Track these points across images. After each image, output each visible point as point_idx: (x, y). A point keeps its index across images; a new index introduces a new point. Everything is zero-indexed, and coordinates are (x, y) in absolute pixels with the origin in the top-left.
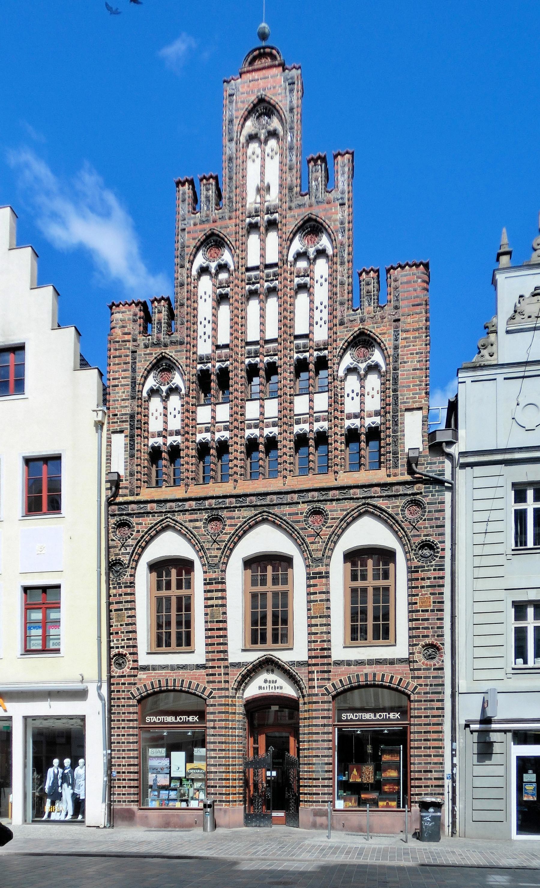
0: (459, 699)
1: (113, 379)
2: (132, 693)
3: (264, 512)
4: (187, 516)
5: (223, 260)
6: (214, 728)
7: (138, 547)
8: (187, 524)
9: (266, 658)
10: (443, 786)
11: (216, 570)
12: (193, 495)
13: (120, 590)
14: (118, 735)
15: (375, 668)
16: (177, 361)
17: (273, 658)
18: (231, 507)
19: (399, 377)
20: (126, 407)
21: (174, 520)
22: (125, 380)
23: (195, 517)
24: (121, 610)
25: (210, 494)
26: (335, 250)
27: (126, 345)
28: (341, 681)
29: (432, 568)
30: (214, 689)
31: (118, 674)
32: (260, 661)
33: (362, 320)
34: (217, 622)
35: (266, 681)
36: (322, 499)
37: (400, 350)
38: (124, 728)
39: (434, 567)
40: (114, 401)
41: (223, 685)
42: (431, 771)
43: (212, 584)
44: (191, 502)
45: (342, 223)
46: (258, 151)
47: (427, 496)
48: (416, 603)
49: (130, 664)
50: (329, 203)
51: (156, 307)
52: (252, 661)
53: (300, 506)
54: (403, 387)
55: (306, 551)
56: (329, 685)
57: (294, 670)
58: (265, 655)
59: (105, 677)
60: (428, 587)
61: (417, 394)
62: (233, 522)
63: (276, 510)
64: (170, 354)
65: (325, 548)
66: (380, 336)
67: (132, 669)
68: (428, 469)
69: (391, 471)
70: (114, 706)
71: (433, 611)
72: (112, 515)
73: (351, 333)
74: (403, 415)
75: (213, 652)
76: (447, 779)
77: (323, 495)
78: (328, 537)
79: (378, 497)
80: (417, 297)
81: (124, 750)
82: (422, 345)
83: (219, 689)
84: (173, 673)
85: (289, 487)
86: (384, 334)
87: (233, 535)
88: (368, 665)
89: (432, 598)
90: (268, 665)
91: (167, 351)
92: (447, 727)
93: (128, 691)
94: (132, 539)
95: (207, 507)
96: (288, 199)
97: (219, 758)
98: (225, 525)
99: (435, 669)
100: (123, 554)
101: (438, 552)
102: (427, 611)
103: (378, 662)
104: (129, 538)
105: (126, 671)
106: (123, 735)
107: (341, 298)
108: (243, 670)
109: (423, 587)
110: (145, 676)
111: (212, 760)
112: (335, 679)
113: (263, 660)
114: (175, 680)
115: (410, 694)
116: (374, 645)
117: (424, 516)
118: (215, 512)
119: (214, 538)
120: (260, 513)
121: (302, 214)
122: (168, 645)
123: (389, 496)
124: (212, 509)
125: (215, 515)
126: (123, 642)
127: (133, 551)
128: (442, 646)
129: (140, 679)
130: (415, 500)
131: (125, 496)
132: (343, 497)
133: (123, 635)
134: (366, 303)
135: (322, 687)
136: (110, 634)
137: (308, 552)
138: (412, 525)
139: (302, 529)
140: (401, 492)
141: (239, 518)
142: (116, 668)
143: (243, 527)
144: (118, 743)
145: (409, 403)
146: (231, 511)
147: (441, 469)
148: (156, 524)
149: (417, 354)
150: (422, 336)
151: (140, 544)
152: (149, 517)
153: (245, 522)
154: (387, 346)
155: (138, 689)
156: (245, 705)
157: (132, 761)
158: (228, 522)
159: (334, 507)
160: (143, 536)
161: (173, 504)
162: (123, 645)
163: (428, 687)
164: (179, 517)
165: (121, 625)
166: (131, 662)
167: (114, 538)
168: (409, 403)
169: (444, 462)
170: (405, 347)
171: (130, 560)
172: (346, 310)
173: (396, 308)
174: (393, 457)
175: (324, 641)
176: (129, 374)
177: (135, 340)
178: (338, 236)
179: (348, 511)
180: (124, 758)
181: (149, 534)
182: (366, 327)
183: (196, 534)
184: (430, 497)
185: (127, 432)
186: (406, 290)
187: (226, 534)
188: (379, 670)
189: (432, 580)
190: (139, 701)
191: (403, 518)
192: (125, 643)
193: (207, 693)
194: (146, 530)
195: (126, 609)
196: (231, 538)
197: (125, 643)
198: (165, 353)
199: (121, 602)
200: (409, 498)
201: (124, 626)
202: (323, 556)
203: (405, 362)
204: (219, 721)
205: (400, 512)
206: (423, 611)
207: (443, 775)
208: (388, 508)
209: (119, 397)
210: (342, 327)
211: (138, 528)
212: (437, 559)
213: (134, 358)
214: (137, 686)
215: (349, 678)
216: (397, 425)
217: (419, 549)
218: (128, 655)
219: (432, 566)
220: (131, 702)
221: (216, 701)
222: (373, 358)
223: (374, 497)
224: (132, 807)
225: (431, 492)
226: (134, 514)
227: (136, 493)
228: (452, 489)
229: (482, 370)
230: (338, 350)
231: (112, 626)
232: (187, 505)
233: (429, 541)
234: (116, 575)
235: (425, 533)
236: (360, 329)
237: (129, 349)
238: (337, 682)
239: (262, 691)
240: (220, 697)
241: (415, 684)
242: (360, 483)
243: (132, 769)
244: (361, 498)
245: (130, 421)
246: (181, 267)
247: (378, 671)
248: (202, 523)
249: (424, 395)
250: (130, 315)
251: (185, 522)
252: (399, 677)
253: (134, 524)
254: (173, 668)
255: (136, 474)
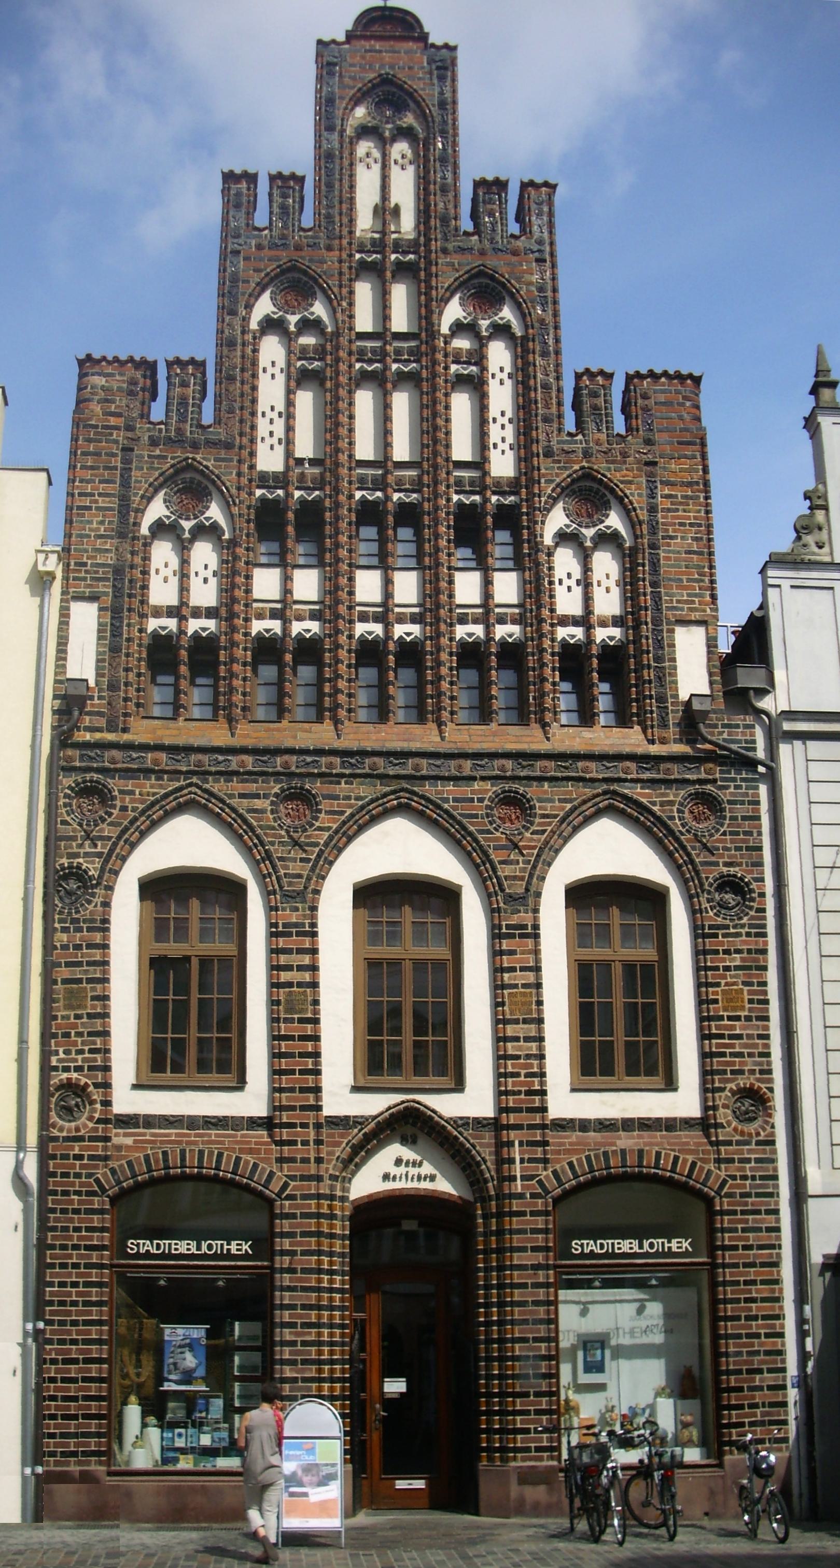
0: (813, 1207)
1: (80, 495)
2: (97, 1181)
3: (402, 790)
4: (235, 784)
5: (313, 314)
6: (292, 1271)
7: (122, 843)
8: (234, 802)
9: (406, 1108)
10: (784, 1404)
11: (300, 905)
12: (249, 743)
13: (78, 935)
14: (62, 1284)
15: (639, 1137)
16: (219, 478)
17: (422, 1108)
18: (331, 775)
19: (662, 562)
20: (107, 551)
21: (206, 791)
22: (107, 499)
23: (252, 787)
24: (80, 981)
25: (289, 743)
26: (531, 331)
27: (111, 434)
28: (571, 1164)
29: (743, 931)
30: (293, 1178)
31: (65, 1134)
32: (392, 1115)
33: (587, 454)
34: (301, 1021)
35: (398, 1162)
36: (522, 774)
37: (659, 515)
38: (76, 1266)
39: (747, 930)
40: (81, 536)
41: (312, 1169)
42: (760, 1371)
43: (289, 934)
44: (245, 757)
45: (541, 289)
46: (376, 154)
47: (727, 787)
48: (716, 1001)
49: (95, 1110)
50: (515, 253)
51: (177, 375)
52: (374, 1113)
53: (476, 786)
54: (670, 579)
55: (491, 879)
56: (545, 1174)
57: (466, 1137)
58: (403, 1102)
59: (32, 1138)
60: (737, 968)
61: (696, 595)
62: (335, 805)
63: (428, 789)
64: (205, 463)
65: (531, 876)
66: (621, 486)
67: (99, 1121)
68: (725, 736)
69: (656, 733)
70: (53, 1211)
71: (748, 1019)
72: (63, 769)
73: (568, 472)
74: (672, 631)
75: (292, 1090)
76: (793, 1387)
77: (523, 767)
78: (536, 852)
79: (632, 781)
80: (687, 430)
81: (74, 1323)
82: (699, 511)
83: (303, 1178)
84: (196, 1135)
85: (452, 745)
86: (630, 482)
87: (336, 832)
88: (624, 1130)
89: (745, 993)
90: (406, 1123)
91: (198, 457)
92: (787, 1271)
93: (89, 1176)
94: (109, 825)
95: (279, 769)
96: (439, 236)
97: (304, 1343)
98: (320, 811)
99: (758, 1143)
100: (87, 855)
101: (753, 900)
102: (738, 1018)
103: (646, 1124)
104: (103, 820)
105: (85, 1126)
106: (75, 1285)
107: (546, 411)
108: (356, 1135)
109: (727, 969)
110: (129, 1141)
111: (287, 1349)
112: (558, 1161)
113: (399, 1112)
114: (201, 1153)
115: (714, 1197)
116: (631, 1086)
117: (722, 825)
118: (296, 782)
119: (295, 835)
120: (393, 792)
121: (468, 264)
122: (178, 1068)
123: (653, 782)
124: (292, 775)
125: (296, 788)
126: (80, 1057)
127: (111, 851)
128: (769, 1094)
129: (119, 1148)
130: (704, 793)
131: (99, 730)
132: (564, 774)
133: (79, 1040)
134: (592, 426)
135: (531, 1178)
136: (46, 1036)
137: (495, 880)
138: (700, 842)
139: (481, 832)
140: (676, 776)
141: (348, 798)
142: (60, 1117)
143: (357, 817)
144: (62, 1303)
145: (682, 609)
146: (331, 783)
147: (748, 738)
148: (166, 796)
149: (691, 525)
150: (699, 497)
151: (126, 836)
152: (149, 779)
153: (362, 808)
154: (636, 505)
155: (113, 1171)
156: (351, 1218)
157: (94, 1351)
158: (325, 805)
159: (546, 792)
160: (135, 819)
161: (205, 758)
162: (80, 1063)
163: (748, 1182)
164: (217, 786)
165: (77, 1017)
166: (98, 1106)
167: (68, 819)
168: (682, 609)
169: (753, 727)
170: (669, 510)
171: (102, 870)
172: (555, 432)
173: (648, 442)
174: (658, 707)
175: (533, 1075)
176: (114, 488)
177: (130, 428)
178: (534, 308)
179: (575, 803)
180: (74, 1342)
181: (150, 816)
182: (595, 467)
183: (255, 824)
184: (732, 790)
185: (108, 601)
186: (664, 415)
187: (320, 829)
188: (653, 1141)
189: (745, 955)
190: (114, 1200)
191: (683, 826)
192: (84, 1060)
193: (276, 1186)
194: (141, 807)
195: (90, 981)
196: (331, 838)
197: (84, 1060)
198: (194, 459)
199: (79, 964)
200: (692, 789)
201: (85, 1020)
202: (527, 890)
203: (671, 538)
204: (304, 1253)
205: (676, 815)
206: (730, 1018)
207: (784, 1379)
208: (654, 803)
209: (90, 530)
210: (550, 460)
211: (123, 800)
212: (752, 913)
213: (127, 461)
214: (111, 1164)
215: (588, 1158)
216: (662, 648)
217: (717, 890)
218: (91, 1088)
219: (743, 926)
220: (96, 1202)
221: (297, 1207)
222: (608, 522)
223: (625, 780)
224: (93, 1467)
225: (734, 780)
226: (116, 770)
227: (121, 726)
228: (773, 779)
229: (810, 570)
230: (543, 499)
231: (55, 1018)
232: (234, 762)
233: (735, 876)
234: (67, 901)
235: (726, 860)
236: (582, 468)
237: (116, 442)
238: (562, 1168)
239: (390, 1186)
240: (305, 1197)
241: (723, 1174)
242: (597, 750)
243: (94, 1370)
244: (597, 780)
245: (115, 579)
246: (228, 314)
247: (646, 1144)
248: (268, 802)
249: (708, 599)
250: (123, 381)
251: (231, 796)
252: (690, 1158)
253: (116, 793)
254: (192, 1122)
255: (123, 688)
